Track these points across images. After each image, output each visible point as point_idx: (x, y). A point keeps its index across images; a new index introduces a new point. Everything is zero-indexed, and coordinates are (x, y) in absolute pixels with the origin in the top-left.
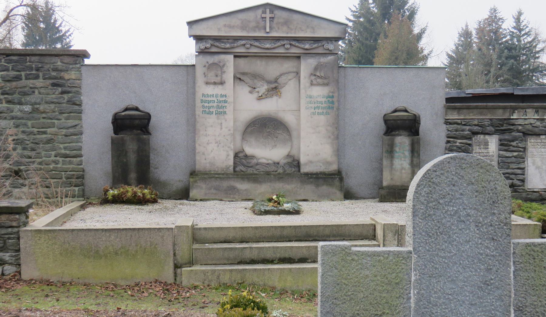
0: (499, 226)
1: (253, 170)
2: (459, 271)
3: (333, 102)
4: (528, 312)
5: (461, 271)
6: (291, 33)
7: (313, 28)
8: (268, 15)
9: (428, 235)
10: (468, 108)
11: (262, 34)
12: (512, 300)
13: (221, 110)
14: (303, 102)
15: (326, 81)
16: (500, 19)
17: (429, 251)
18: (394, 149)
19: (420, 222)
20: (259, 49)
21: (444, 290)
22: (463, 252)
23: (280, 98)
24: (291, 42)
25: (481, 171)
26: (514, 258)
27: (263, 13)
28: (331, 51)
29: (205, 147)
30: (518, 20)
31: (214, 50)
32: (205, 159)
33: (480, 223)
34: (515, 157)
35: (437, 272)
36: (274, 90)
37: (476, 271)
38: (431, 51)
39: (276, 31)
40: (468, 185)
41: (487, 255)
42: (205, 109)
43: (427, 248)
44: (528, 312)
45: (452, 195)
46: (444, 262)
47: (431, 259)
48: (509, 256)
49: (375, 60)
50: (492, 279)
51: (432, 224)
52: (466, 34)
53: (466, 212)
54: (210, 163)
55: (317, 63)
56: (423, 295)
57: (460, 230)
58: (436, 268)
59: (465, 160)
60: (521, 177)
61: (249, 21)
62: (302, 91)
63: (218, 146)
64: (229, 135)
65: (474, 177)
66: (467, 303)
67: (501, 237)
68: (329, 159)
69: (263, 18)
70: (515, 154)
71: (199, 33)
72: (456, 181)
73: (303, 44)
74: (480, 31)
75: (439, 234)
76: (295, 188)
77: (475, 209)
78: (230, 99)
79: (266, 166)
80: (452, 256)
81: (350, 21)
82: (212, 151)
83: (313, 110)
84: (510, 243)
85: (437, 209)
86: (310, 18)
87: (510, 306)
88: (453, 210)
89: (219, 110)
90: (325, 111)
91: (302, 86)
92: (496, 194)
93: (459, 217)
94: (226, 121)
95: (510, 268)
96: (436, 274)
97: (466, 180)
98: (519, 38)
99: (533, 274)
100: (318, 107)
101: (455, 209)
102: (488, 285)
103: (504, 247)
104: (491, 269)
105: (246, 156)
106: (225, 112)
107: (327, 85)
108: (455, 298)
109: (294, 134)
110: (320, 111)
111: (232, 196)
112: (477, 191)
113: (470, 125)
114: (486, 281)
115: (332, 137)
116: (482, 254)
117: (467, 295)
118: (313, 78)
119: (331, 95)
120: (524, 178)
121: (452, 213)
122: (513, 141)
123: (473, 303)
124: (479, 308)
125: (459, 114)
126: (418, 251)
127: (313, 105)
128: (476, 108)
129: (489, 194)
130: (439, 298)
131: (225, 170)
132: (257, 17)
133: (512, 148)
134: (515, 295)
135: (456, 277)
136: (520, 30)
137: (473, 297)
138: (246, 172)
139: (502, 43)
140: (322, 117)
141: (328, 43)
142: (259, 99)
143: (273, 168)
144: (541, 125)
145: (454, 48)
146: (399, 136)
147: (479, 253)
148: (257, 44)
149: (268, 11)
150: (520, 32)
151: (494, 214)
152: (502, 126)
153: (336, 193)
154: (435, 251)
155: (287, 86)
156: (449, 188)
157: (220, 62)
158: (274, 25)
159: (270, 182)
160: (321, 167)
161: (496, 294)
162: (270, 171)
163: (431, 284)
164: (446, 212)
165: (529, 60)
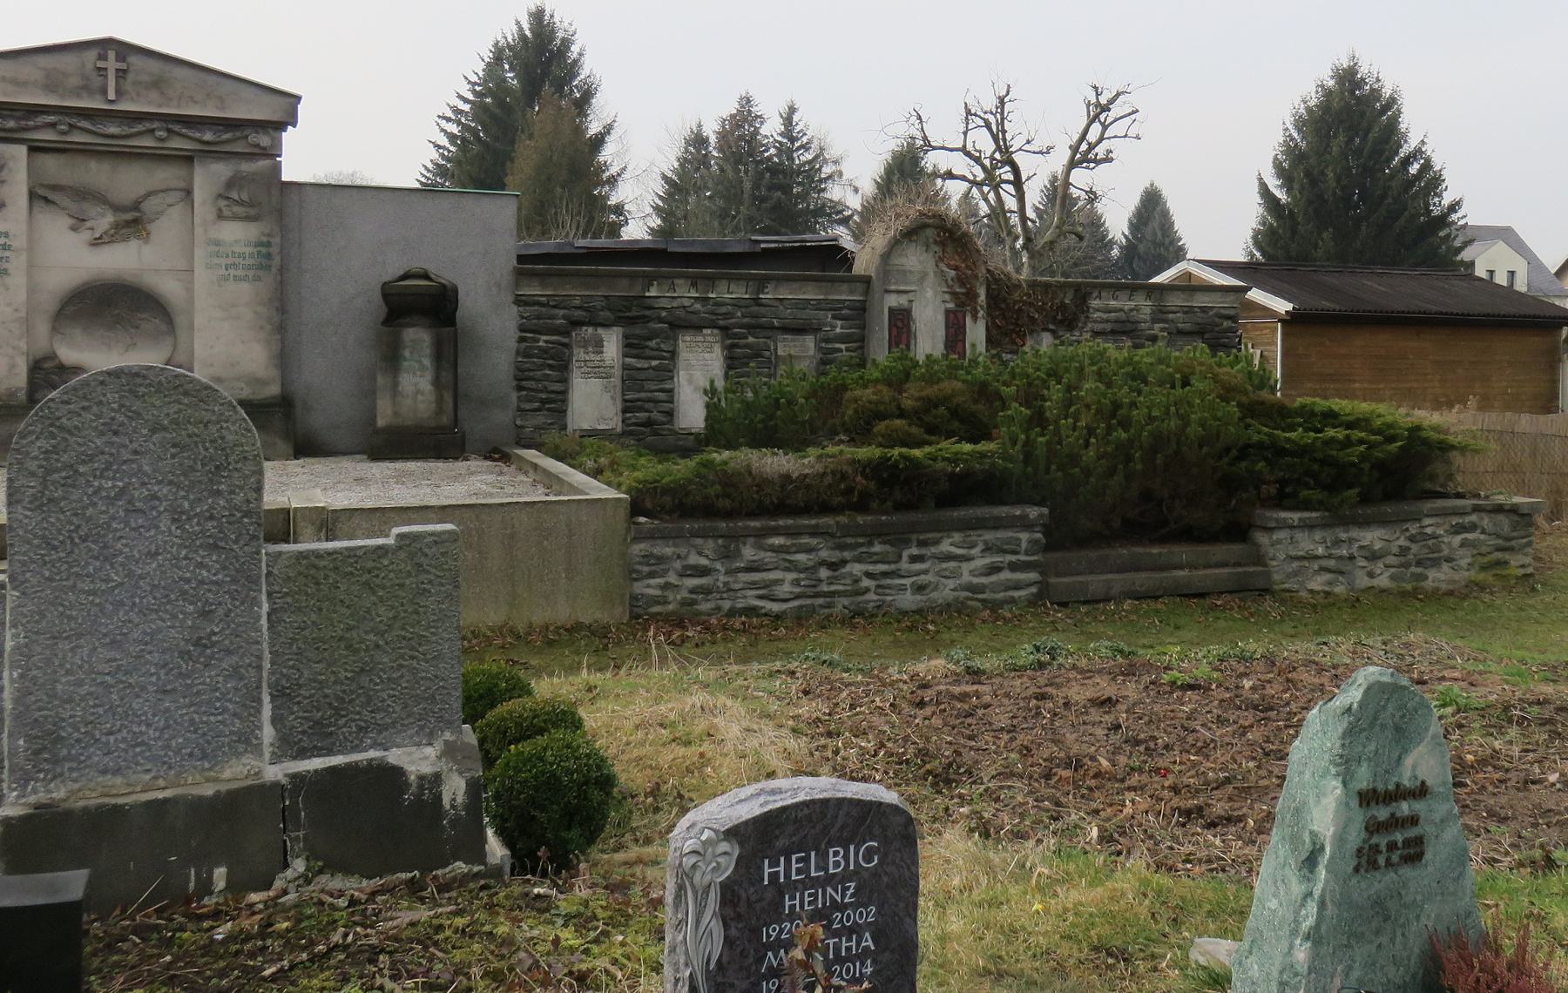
0: (232, 519)
2: (130, 621)
3: (269, 256)
4: (305, 698)
5: (137, 620)
7: (221, 99)
8: (112, 64)
9: (48, 544)
10: (560, 274)
11: (96, 104)
12: (265, 674)
14: (199, 253)
15: (252, 212)
16: (757, 117)
17: (51, 579)
19: (26, 517)
21: (90, 665)
22: (141, 577)
24: (170, 126)
25: (186, 401)
26: (268, 584)
28: (264, 149)
30: (788, 120)
33: (182, 513)
34: (654, 369)
35: (73, 625)
37: (174, 617)
38: (624, 169)
40: (153, 431)
41: (202, 582)
43: (47, 574)
44: (305, 698)
45: (112, 455)
46: (92, 602)
47: (57, 597)
48: (256, 582)
49: (509, 180)
50: (215, 634)
51: (58, 519)
52: (698, 140)
53: (148, 490)
56: (34, 680)
57: (133, 529)
58: (70, 618)
59: (145, 377)
60: (666, 406)
62: (198, 231)
65: (168, 415)
66: (151, 688)
67: (236, 542)
69: (99, 69)
70: (655, 363)
72: (122, 424)
73: (199, 131)
74: (723, 135)
75: (77, 540)
77: (171, 483)
78: (19, 242)
80: (114, 588)
81: (466, 100)
83: (223, 271)
84: (258, 553)
85: (73, 486)
86: (212, 79)
87: (259, 687)
88: (114, 486)
91: (197, 220)
92: (223, 449)
93: (130, 502)
95: (260, 607)
96: (71, 630)
97: (147, 421)
98: (789, 153)
99: (314, 617)
101: (120, 484)
102: (205, 646)
103: (244, 563)
104: (211, 611)
108: (122, 682)
109: (180, 321)
110: (240, 273)
112: (174, 446)
113: (565, 308)
114: (200, 638)
116: (188, 581)
117: (153, 671)
118: (222, 203)
120: (673, 410)
121: (113, 494)
122: (650, 339)
123: (169, 687)
124: (184, 697)
125: (543, 286)
126: (23, 583)
127: (223, 261)
128: (577, 274)
129: (207, 449)
130: (80, 683)
132: (84, 65)
133: (648, 352)
134: (273, 663)
135: (125, 634)
136: (793, 140)
137: (167, 674)
139: (761, 162)
140: (245, 286)
142: (93, 245)
144: (702, 309)
145: (676, 165)
147: (181, 579)
150: (793, 143)
151: (219, 493)
152: (630, 310)
154: (66, 580)
156: (104, 439)
158: (128, 86)
161: (224, 665)
163: (56, 655)
164: (95, 493)
165: (808, 194)
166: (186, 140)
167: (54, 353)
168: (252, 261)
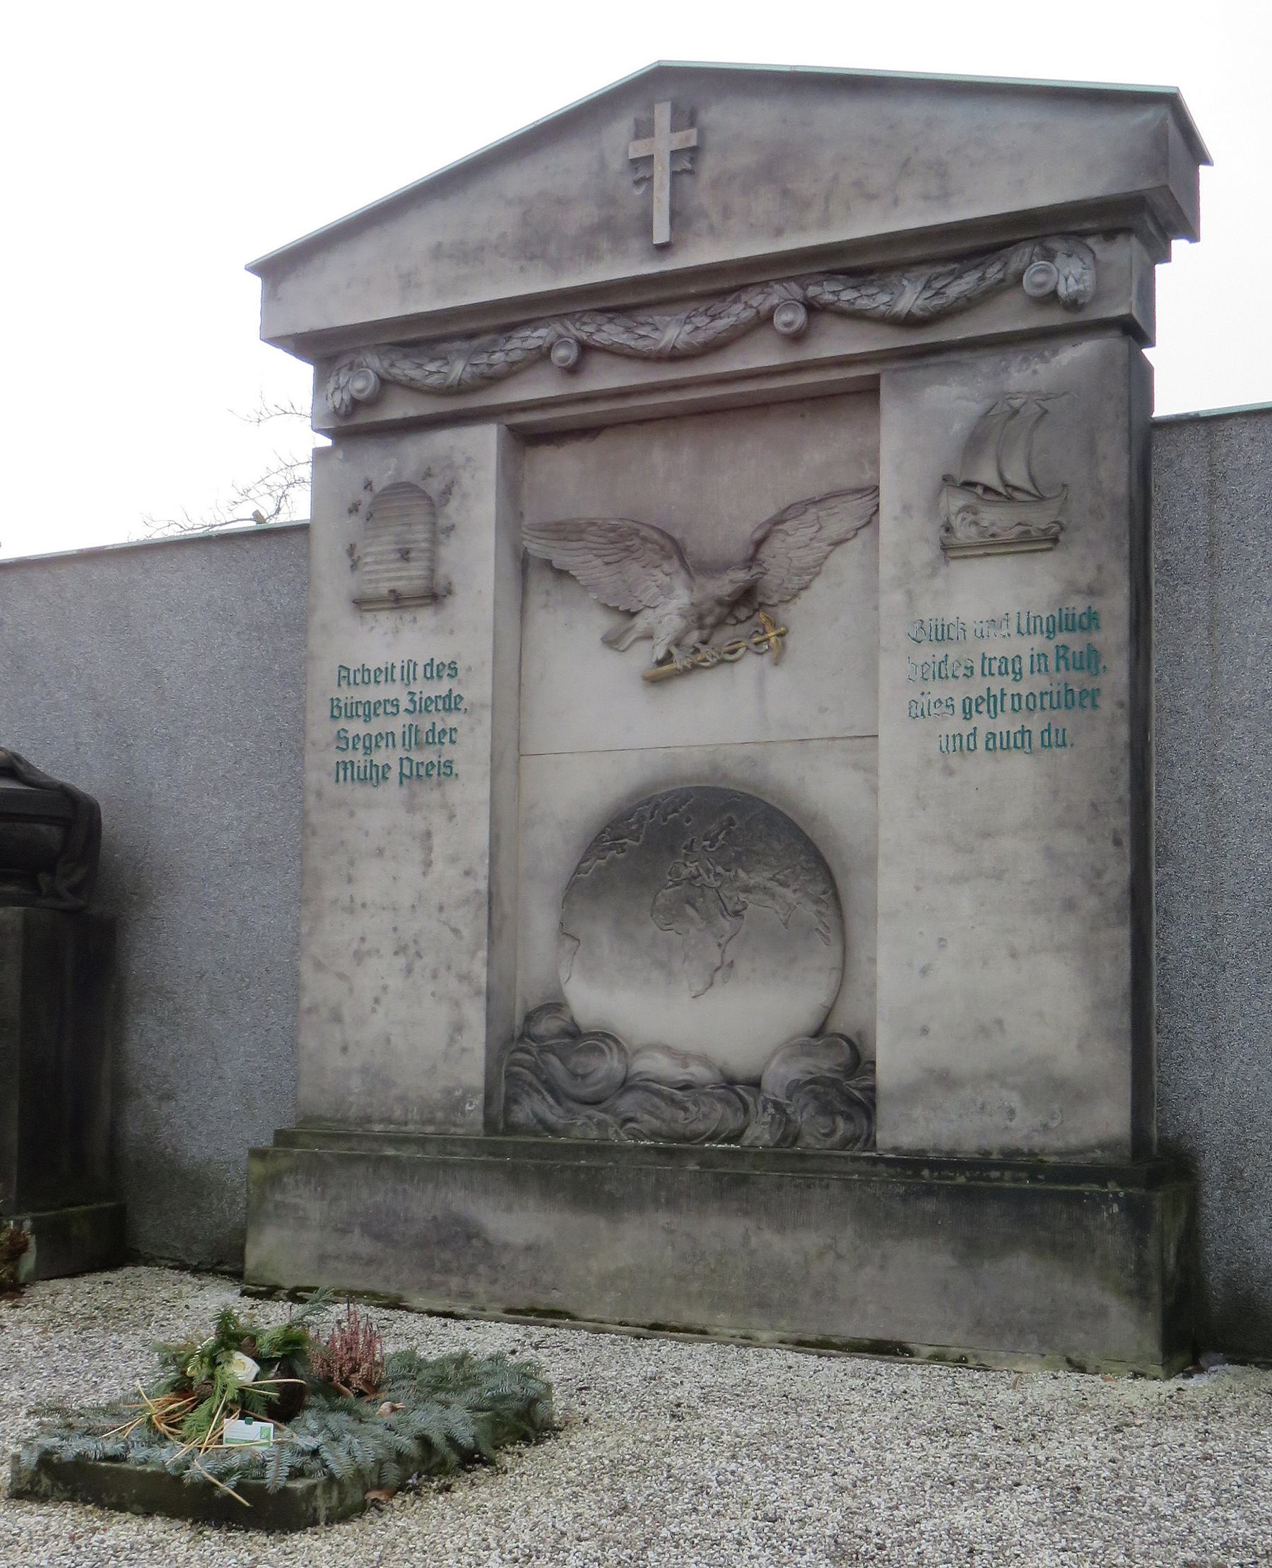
1: (601, 1125)
3: (1091, 660)
6: (802, 228)
13: (428, 755)
20: (637, 366)
23: (777, 662)
24: (813, 291)
27: (637, 136)
28: (1073, 305)
29: (341, 976)
31: (400, 408)
32: (345, 1049)
36: (743, 613)
39: (712, 229)
42: (348, 756)
54: (365, 1070)
55: (988, 402)
61: (563, 202)
62: (892, 600)
63: (409, 970)
64: (466, 901)
68: (1069, 1061)
71: (313, 320)
76: (821, 1255)
79: (672, 1101)
82: (377, 1001)
83: (955, 724)
86: (914, 112)
89: (416, 757)
90: (1036, 724)
94: (452, 817)
100: (992, 703)
105: (574, 1033)
106: (449, 764)
107: (1051, 540)
109: (853, 889)
110: (1005, 723)
111: (455, 1282)
115: (1091, 903)
118: (957, 501)
119: (1081, 609)
127: (957, 691)
131: (440, 1115)
138: (565, 1132)
141: (1050, 256)
143: (718, 1115)
148: (612, 333)
149: (663, 115)
153: (1102, 1313)
155: (818, 584)
157: (428, 474)
158: (701, 195)
159: (672, 1204)
160: (1012, 1113)
162: (697, 1136)
166: (866, 328)
167: (560, 992)
168: (1040, 683)
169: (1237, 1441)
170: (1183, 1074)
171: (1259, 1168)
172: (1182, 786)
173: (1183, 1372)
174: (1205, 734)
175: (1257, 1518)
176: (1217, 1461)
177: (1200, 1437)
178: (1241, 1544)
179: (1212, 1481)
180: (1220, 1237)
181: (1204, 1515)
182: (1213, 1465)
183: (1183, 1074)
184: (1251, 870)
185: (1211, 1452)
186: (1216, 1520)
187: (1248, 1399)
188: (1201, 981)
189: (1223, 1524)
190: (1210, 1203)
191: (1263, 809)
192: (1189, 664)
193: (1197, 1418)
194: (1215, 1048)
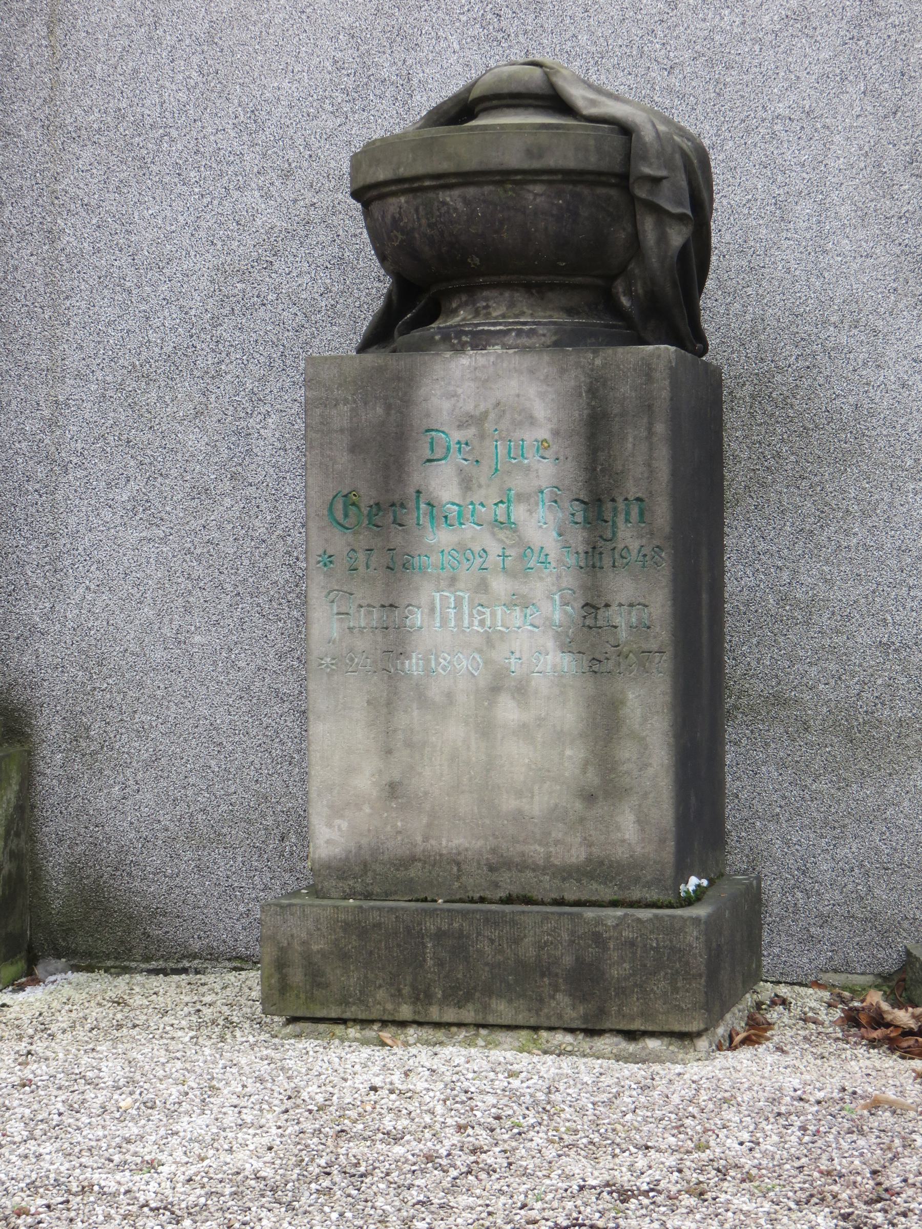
18: (416, 479)
146: (460, 349)
169: (66, 1061)
170: (15, 606)
171: (108, 723)
172: (13, 231)
173: (13, 985)
174: (43, 163)
175: (77, 1149)
176: (38, 1087)
177: (20, 1060)
178: (52, 1182)
179: (27, 1112)
180: (61, 813)
181: (12, 1152)
182: (32, 1092)
183: (15, 606)
184: (99, 342)
185: (31, 1076)
186: (26, 1157)
187: (87, 1011)
188: (37, 486)
189: (34, 1160)
190: (48, 771)
191: (116, 263)
192: (23, 70)
193: (20, 1038)
194: (55, 571)
